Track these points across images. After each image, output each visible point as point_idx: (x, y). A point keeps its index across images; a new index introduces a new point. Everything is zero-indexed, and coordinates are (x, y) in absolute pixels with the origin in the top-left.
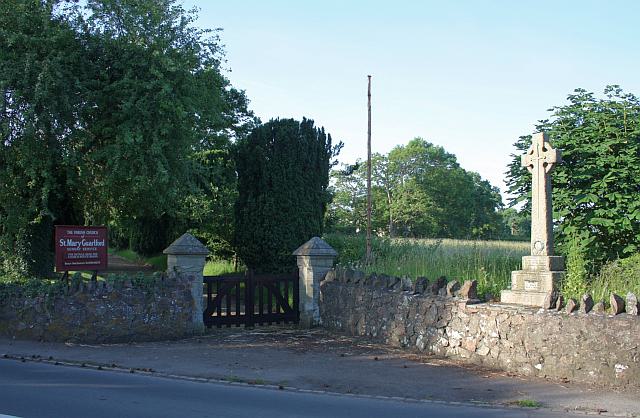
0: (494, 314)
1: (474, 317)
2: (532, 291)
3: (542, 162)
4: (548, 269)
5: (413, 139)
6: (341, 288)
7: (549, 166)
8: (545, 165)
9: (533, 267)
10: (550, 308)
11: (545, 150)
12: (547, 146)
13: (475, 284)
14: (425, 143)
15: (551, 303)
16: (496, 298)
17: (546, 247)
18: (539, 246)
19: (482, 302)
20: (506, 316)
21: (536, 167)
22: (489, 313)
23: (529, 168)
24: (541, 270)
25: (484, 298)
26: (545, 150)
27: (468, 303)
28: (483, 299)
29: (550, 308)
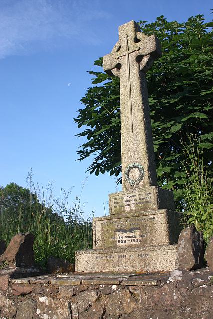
0: (65, 292)
1: (25, 304)
2: (130, 247)
3: (134, 55)
4: (155, 206)
5: (9, 184)
6: (175, 297)
7: (145, 60)
8: (139, 59)
9: (127, 209)
10: (194, 268)
11: (136, 41)
12: (140, 35)
13: (29, 242)
14: (17, 186)
15: (195, 254)
16: (68, 266)
17: (147, 174)
18: (135, 173)
19: (42, 273)
20: (93, 296)
21: (125, 67)
22: (54, 293)
23: (114, 72)
24: (143, 207)
25: (47, 264)
26: (136, 41)
27: (15, 276)
28: (46, 269)
29: (194, 268)
